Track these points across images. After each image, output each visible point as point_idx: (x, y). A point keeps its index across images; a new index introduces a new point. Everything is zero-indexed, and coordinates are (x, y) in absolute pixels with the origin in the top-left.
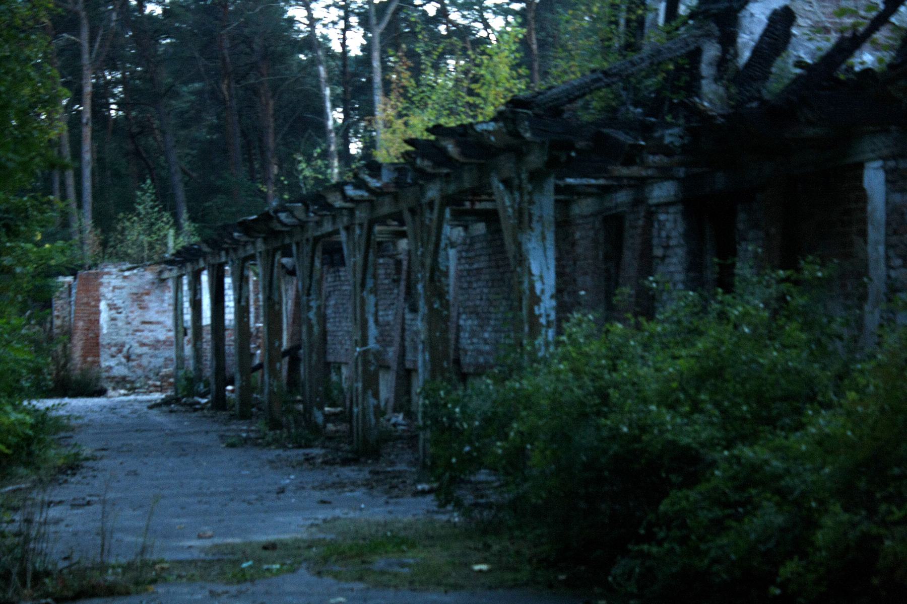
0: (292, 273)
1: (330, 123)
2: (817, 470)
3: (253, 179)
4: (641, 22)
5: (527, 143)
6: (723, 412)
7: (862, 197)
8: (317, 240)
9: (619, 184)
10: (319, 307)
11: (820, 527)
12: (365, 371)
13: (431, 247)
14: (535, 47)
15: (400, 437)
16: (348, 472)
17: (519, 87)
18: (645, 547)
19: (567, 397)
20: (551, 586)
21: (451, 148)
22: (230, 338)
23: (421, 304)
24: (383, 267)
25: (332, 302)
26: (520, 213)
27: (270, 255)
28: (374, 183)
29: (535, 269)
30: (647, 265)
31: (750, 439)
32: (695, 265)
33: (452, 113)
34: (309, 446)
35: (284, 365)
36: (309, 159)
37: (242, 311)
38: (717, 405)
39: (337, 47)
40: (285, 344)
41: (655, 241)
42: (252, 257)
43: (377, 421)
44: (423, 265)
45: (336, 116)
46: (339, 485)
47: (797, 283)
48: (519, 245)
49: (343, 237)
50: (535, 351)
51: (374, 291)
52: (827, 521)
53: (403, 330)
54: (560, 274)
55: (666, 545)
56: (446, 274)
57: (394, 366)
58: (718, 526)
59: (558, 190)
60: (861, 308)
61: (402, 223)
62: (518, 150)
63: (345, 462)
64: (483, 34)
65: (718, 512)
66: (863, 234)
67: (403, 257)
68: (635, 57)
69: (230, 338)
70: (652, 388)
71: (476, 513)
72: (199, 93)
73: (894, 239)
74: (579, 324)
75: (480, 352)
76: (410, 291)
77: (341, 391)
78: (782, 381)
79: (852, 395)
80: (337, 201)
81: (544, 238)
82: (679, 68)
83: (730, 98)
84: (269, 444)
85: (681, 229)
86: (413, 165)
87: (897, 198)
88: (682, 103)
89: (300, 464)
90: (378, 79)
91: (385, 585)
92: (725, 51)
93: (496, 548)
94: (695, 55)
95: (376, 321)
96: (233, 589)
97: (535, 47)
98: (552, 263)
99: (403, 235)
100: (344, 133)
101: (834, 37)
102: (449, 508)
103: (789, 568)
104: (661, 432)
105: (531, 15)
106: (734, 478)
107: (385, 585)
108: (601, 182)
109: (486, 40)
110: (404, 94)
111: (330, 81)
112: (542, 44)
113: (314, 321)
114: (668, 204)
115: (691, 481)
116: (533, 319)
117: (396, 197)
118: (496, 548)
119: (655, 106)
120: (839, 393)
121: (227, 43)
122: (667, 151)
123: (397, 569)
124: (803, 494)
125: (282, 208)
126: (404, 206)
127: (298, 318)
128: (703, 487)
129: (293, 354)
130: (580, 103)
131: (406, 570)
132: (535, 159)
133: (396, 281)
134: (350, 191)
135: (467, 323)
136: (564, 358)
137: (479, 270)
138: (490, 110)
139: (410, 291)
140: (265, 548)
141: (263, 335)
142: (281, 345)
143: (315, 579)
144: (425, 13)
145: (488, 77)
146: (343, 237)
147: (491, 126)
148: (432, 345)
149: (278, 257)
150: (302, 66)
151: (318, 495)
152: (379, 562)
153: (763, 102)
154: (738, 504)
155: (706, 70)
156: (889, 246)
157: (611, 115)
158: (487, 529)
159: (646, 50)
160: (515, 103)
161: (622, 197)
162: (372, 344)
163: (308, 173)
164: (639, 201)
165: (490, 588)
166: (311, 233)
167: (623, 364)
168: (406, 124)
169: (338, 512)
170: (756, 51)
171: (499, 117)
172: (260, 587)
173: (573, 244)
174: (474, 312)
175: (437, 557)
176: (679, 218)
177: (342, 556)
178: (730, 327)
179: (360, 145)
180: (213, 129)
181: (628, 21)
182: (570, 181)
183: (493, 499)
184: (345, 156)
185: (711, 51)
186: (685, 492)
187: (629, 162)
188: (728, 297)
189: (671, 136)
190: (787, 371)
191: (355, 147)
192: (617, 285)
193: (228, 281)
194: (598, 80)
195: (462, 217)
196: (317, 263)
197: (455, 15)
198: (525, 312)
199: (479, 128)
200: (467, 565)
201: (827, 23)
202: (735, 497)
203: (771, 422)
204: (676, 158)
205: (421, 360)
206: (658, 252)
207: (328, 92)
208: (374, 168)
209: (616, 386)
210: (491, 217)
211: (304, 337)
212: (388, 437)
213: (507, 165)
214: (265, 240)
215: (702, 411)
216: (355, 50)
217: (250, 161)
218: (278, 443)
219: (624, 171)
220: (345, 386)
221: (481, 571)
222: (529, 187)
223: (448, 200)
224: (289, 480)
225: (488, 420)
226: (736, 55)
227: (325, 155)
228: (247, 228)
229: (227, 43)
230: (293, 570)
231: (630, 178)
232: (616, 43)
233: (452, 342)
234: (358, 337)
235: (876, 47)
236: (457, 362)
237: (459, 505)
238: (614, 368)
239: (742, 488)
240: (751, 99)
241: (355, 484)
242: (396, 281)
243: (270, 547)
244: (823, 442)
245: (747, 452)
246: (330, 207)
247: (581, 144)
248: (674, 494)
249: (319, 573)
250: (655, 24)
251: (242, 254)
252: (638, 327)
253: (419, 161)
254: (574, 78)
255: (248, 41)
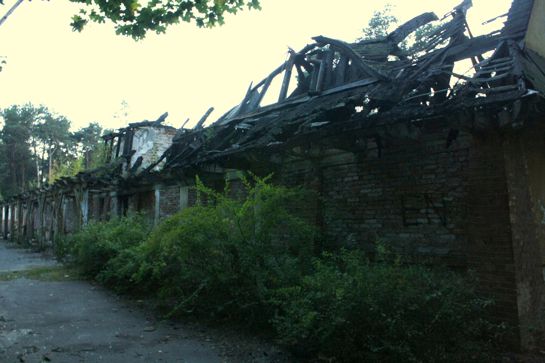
0: (26, 208)
1: (38, 174)
2: (141, 255)
3: (18, 186)
4: (110, 157)
5: (82, 182)
6: (123, 242)
7: (155, 197)
8: (32, 201)
9: (103, 192)
10: (32, 216)
11: (141, 266)
12: (42, 231)
13: (59, 204)
14: (88, 160)
15: (51, 247)
16: (37, 255)
17: (83, 169)
18: (104, 271)
19: (88, 238)
20: (83, 280)
21: (65, 182)
22: (9, 223)
23: (56, 216)
24: (49, 208)
25: (35, 215)
26: (80, 197)
27: (21, 204)
28: (47, 189)
29: (83, 209)
30: (109, 209)
31: (127, 247)
32: (119, 210)
33: (67, 174)
34: (27, 248)
35: (23, 230)
36: (32, 182)
37: (13, 217)
38: (121, 240)
39: (41, 157)
40: (24, 224)
41: (111, 204)
42: (16, 204)
43: (45, 243)
44: (57, 207)
45: (40, 173)
46: (34, 257)
47: (140, 215)
48: (80, 204)
49: (39, 200)
50: (82, 228)
51: (46, 213)
52: (143, 265)
53: (52, 222)
54: (89, 211)
55: (109, 271)
56: (63, 210)
57: (50, 230)
58: (120, 266)
59: (89, 192)
60: (153, 220)
61: (53, 197)
62: (80, 183)
63: (36, 252)
64: (76, 157)
65: (120, 263)
66: (155, 205)
67: (53, 206)
68: (108, 164)
69: (9, 223)
70: (107, 237)
71: (67, 264)
72: (6, 166)
73: (161, 206)
74: (92, 222)
75: (70, 227)
76: (54, 213)
77: (37, 236)
78: (135, 236)
79: (149, 239)
80: (37, 192)
81: (85, 203)
82: (118, 168)
83: (128, 174)
84: (17, 248)
85: (117, 201)
86: (56, 185)
87: (162, 198)
88: (117, 175)
89: (25, 252)
90: (50, 165)
91: (339, 153)
92: (128, 164)
93: (70, 272)
94: (121, 165)
95: (46, 220)
96: (4, 282)
97: (88, 160)
98: (87, 208)
99: (53, 200)
100: (42, 177)
101: (150, 164)
102: (60, 262)
103: (134, 276)
104: (109, 246)
105: (87, 154)
106: (124, 256)
107: (339, 153)
108: (99, 191)
109: (76, 159)
110: (56, 169)
111: (39, 164)
112: (89, 160)
113: (30, 219)
114: (114, 196)
115: (115, 256)
116: (82, 221)
117: (52, 192)
118: (70, 272)
119: (112, 176)
120: (147, 239)
121: (14, 155)
122: (114, 185)
123: (46, 277)
124: (138, 260)
125: (24, 193)
126: (54, 194)
127: (27, 219)
128: (116, 258)
129: (25, 227)
130: (96, 173)
131: (48, 277)
132: (84, 186)
133: (52, 211)
134: (41, 190)
135: (67, 221)
136: (88, 229)
137: (71, 209)
138: (76, 174)
139: (54, 213)
140: (14, 272)
141: (18, 222)
142: (22, 224)
143: (26, 280)
144: (63, 151)
145: (75, 166)
146: (39, 200)
147: (75, 178)
148: (58, 226)
149: (22, 204)
150: (32, 161)
151: (28, 260)
152: (42, 275)
153: (135, 176)
154: (124, 262)
155: (124, 168)
156: (160, 207)
157: (103, 177)
158: (69, 267)
159: (111, 163)
160: (80, 173)
161: (104, 194)
162: (44, 225)
163: (32, 185)
164: (107, 196)
165: (69, 281)
166: (31, 199)
167: (101, 231)
168: (56, 176)
169: (33, 264)
170: (135, 165)
171: (76, 176)
172: (12, 282)
173: (93, 204)
174: (69, 218)
175: (56, 274)
176: (116, 200)
177: (33, 274)
178: (125, 224)
179: (45, 179)
180: (9, 174)
181: (107, 157)
182: (93, 190)
183: (71, 261)
184: (41, 181)
185: (125, 164)
186: (113, 259)
187: (105, 187)
188: (125, 217)
189: (115, 182)
190: (136, 233)
191: (44, 180)
192: (102, 213)
193: (10, 210)
194: (99, 169)
195: (68, 197)
196: (32, 206)
197: (70, 152)
198: (80, 219)
199: (72, 178)
200: (63, 276)
201: (150, 160)
202: (124, 260)
203: (133, 244)
204: (116, 187)
205: (56, 229)
206: (111, 207)
207: (38, 167)
208: (47, 185)
209: (99, 236)
210: (74, 197)
211: (28, 223)
212: (47, 247)
213: (78, 186)
214: (20, 201)
215: (118, 242)
216: (46, 158)
217: (18, 182)
218: (20, 248)
219: (105, 189)
220: (38, 234)
221: (67, 277)
222: (83, 192)
223: (64, 193)
224: (22, 256)
225: (70, 243)
226: (130, 166)
227: (36, 181)
228: (15, 197)
229: (14, 155)
230: (20, 277)
231: (106, 190)
232: (105, 161)
233: (64, 225)
234: (41, 223)
235: (160, 166)
236: (65, 229)
237: (62, 262)
238: (99, 232)
239: (126, 258)
240: (133, 175)
241: (38, 257)
242: (52, 211)
243: (15, 272)
244: (143, 248)
245: (127, 251)
246: (36, 194)
247: (95, 183)
248: (111, 260)
249: (27, 278)
250: (113, 158)
251: (13, 203)
252: (105, 223)
253: (57, 184)
254: (95, 168)
255: (19, 154)
